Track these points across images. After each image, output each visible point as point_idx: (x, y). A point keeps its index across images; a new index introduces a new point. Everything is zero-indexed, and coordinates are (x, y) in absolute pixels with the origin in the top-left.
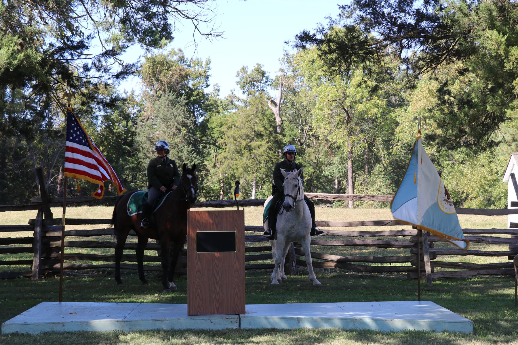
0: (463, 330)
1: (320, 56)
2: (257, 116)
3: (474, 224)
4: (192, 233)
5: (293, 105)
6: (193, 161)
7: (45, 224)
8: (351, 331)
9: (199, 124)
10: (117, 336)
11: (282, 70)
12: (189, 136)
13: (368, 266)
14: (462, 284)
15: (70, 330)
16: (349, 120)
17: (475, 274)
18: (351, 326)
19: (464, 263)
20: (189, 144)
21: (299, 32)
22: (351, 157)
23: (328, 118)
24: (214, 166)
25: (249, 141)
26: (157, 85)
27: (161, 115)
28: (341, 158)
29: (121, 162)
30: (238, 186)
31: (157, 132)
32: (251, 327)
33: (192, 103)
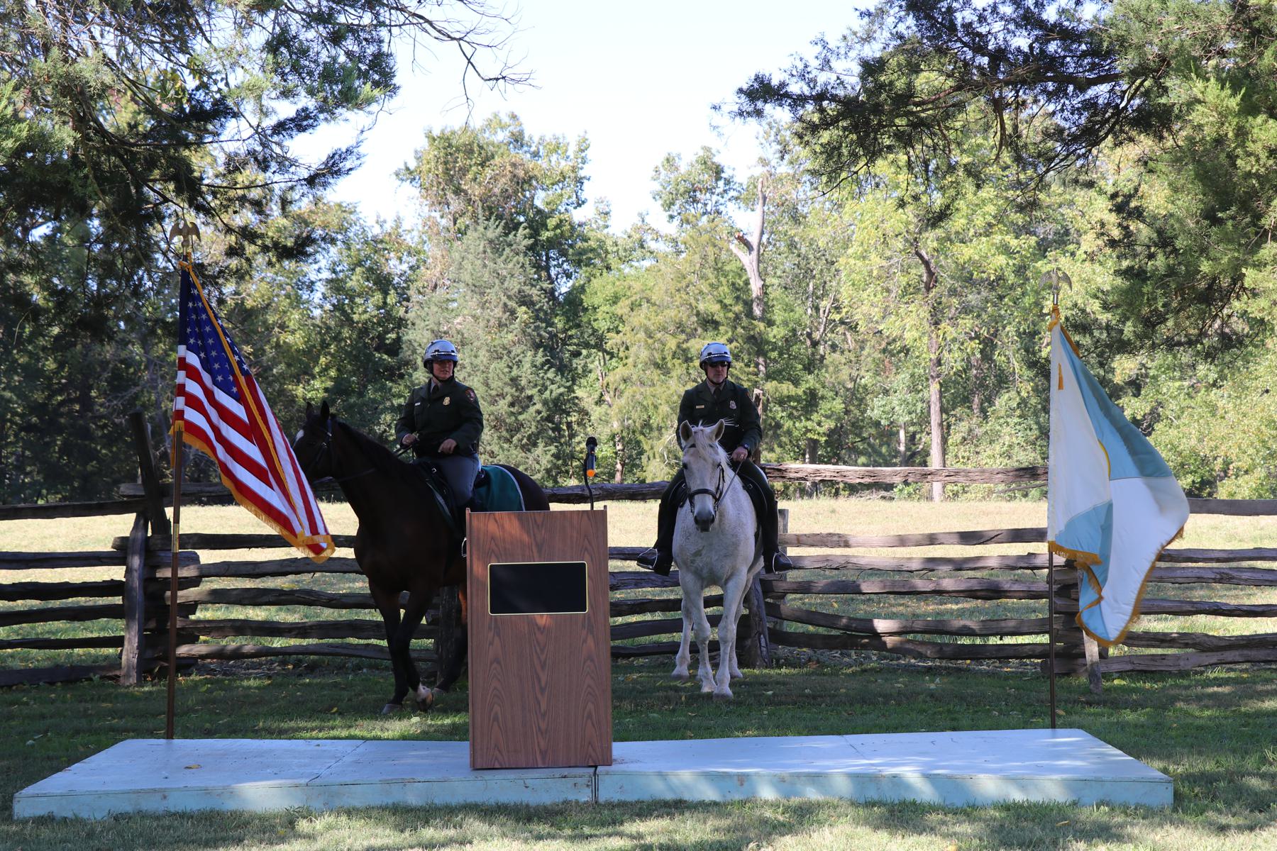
0: (1146, 801)
1: (801, 137)
2: (703, 277)
3: (1231, 537)
4: (479, 570)
5: (792, 245)
6: (546, 389)
7: (154, 548)
8: (870, 804)
9: (561, 299)
10: (291, 823)
11: (764, 162)
12: (537, 328)
13: (948, 645)
14: (1179, 687)
15: (180, 808)
16: (932, 279)
17: (1214, 660)
18: (873, 794)
19: (1183, 635)
20: (537, 346)
21: (745, 82)
22: (938, 376)
23: (879, 278)
24: (600, 401)
25: (683, 337)
26: (456, 204)
27: (466, 277)
28: (912, 375)
29: (371, 394)
30: (593, 449)
31: (459, 319)
32: (623, 798)
33: (543, 246)
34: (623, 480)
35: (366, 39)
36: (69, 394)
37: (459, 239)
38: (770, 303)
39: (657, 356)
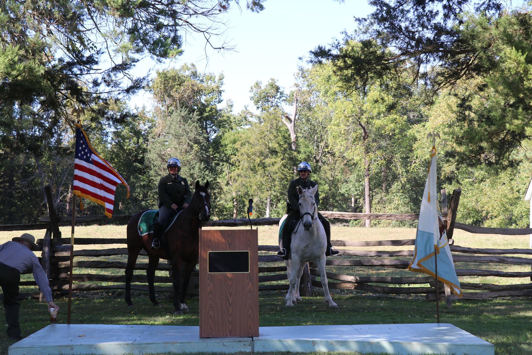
3: (495, 244)
5: (308, 120)
11: (297, 85)
12: (202, 153)
14: (482, 306)
17: (497, 295)
19: (484, 284)
20: (201, 161)
23: (344, 134)
25: (263, 158)
26: (168, 101)
27: (172, 131)
28: (358, 175)
31: (169, 149)
34: (236, 217)
35: (170, 30)
36: (4, 179)
37: (170, 116)
38: (299, 144)
39: (252, 165)
